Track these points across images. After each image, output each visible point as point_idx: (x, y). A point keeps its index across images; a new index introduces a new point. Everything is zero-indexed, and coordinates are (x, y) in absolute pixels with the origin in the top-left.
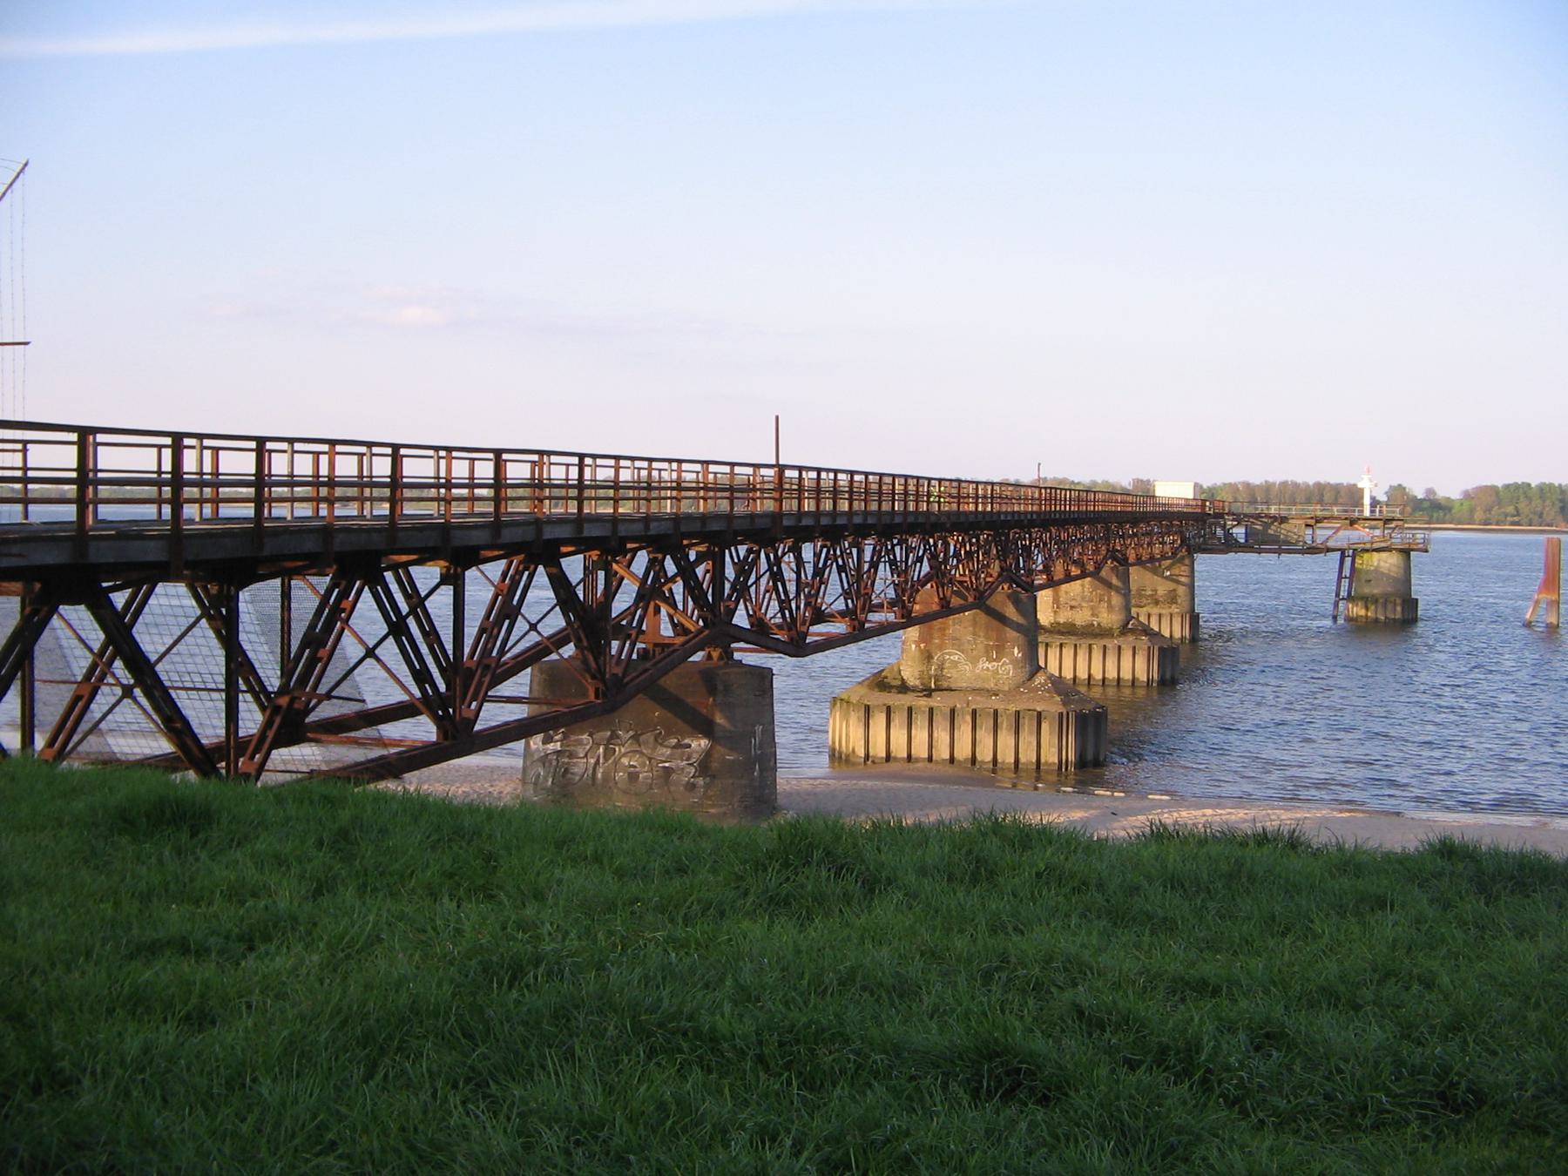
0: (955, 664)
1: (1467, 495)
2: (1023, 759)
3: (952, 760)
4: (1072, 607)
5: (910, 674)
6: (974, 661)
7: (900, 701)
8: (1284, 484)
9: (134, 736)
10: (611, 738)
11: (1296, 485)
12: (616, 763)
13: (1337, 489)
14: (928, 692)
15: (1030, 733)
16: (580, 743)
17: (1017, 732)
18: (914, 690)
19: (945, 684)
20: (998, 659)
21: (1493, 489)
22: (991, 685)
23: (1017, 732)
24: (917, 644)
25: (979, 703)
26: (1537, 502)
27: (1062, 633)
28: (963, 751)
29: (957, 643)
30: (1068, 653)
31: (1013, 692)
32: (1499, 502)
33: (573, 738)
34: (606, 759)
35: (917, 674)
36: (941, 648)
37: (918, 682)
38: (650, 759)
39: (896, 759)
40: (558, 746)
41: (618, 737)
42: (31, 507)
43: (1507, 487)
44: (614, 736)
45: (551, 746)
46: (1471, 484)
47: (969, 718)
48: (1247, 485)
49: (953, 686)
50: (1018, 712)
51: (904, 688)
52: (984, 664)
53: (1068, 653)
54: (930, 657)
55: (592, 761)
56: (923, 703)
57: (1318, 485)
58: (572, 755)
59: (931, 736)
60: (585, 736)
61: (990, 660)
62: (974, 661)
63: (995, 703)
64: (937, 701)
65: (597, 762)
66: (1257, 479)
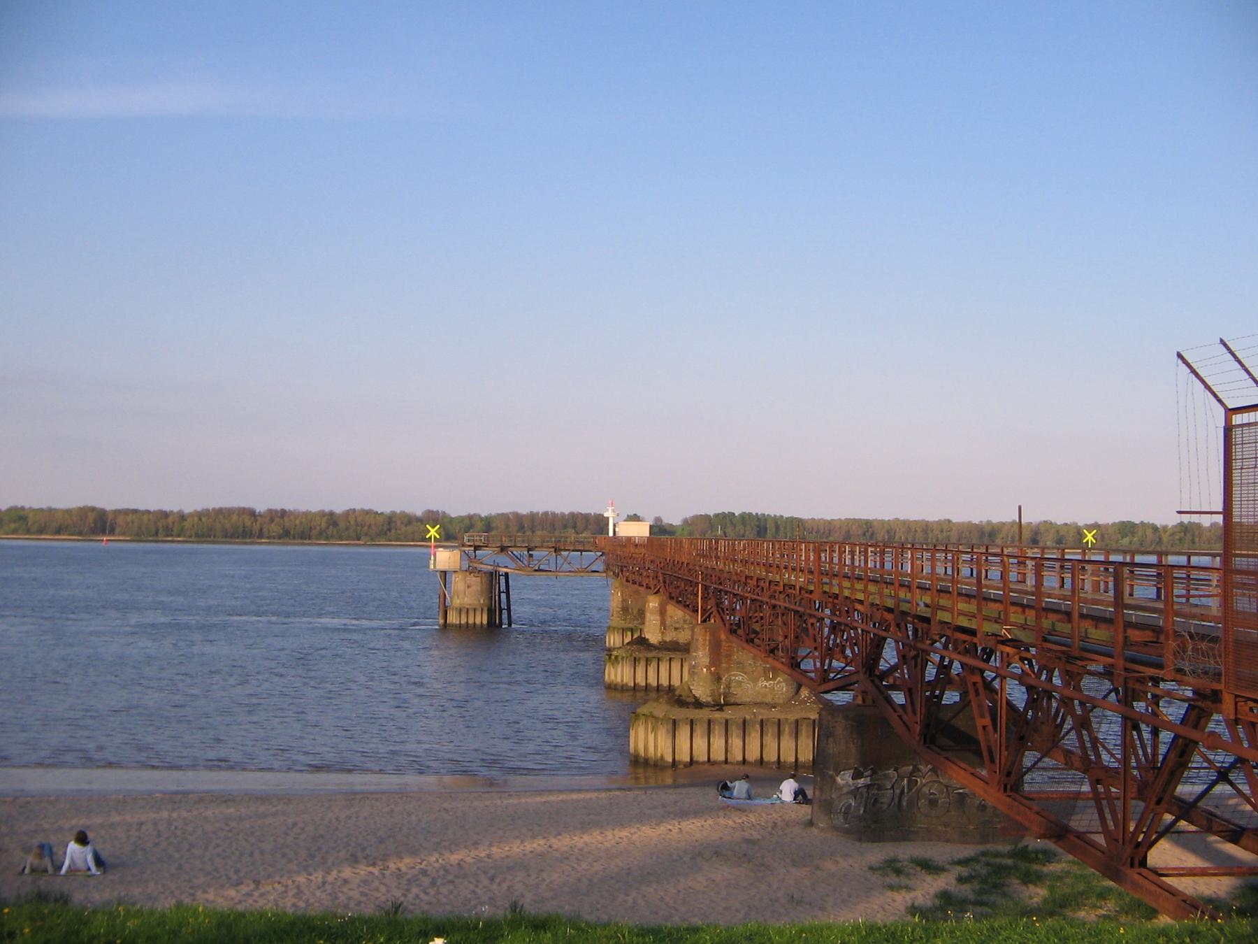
0: (740, 683)
1: (685, 521)
2: (801, 759)
3: (744, 761)
4: (676, 629)
5: (701, 691)
6: (755, 680)
7: (704, 714)
8: (546, 514)
9: (210, 768)
10: (913, 771)
11: (554, 515)
12: (918, 791)
13: (586, 518)
14: (720, 707)
15: (808, 737)
16: (887, 777)
17: (797, 738)
18: (707, 705)
19: (732, 700)
20: (774, 678)
21: (707, 517)
22: (769, 699)
23: (797, 738)
24: (708, 668)
25: (764, 714)
26: (740, 528)
27: (669, 650)
28: (753, 754)
29: (741, 666)
30: (676, 667)
31: (787, 705)
32: (335, 524)
33: (881, 773)
34: (910, 790)
35: (708, 692)
36: (728, 670)
37: (709, 699)
38: (947, 787)
39: (697, 763)
40: (868, 781)
41: (919, 770)
42: (1185, 563)
43: (717, 516)
44: (916, 769)
45: (861, 781)
46: (689, 514)
47: (758, 727)
48: (516, 515)
49: (738, 701)
50: (797, 721)
51: (698, 704)
52: (763, 683)
53: (676, 667)
54: (719, 679)
55: (898, 791)
56: (717, 715)
57: (572, 515)
58: (880, 788)
59: (726, 742)
60: (891, 771)
61: (767, 679)
62: (755, 680)
63: (775, 714)
64: (729, 713)
65: (902, 792)
66: (524, 510)
